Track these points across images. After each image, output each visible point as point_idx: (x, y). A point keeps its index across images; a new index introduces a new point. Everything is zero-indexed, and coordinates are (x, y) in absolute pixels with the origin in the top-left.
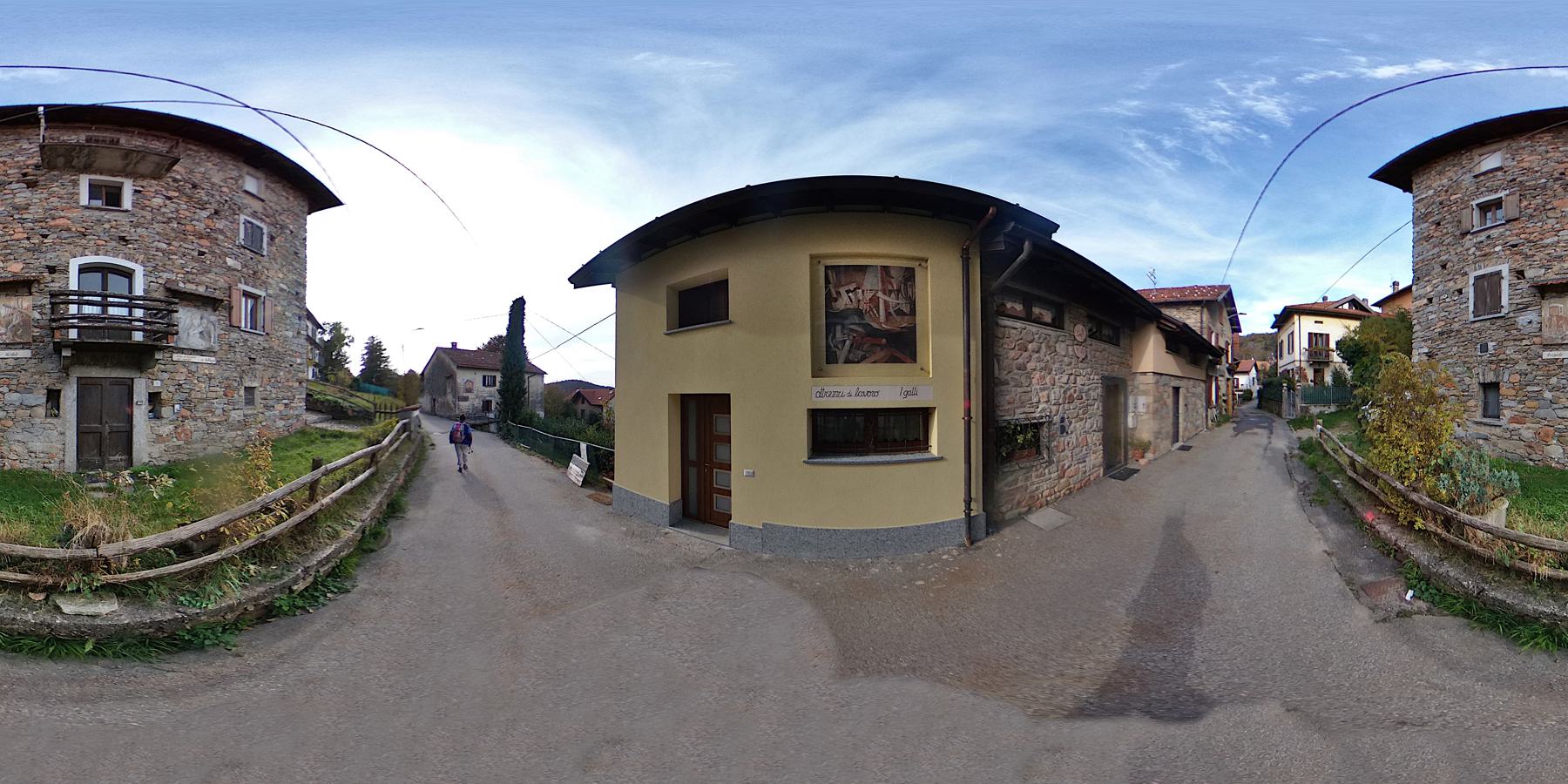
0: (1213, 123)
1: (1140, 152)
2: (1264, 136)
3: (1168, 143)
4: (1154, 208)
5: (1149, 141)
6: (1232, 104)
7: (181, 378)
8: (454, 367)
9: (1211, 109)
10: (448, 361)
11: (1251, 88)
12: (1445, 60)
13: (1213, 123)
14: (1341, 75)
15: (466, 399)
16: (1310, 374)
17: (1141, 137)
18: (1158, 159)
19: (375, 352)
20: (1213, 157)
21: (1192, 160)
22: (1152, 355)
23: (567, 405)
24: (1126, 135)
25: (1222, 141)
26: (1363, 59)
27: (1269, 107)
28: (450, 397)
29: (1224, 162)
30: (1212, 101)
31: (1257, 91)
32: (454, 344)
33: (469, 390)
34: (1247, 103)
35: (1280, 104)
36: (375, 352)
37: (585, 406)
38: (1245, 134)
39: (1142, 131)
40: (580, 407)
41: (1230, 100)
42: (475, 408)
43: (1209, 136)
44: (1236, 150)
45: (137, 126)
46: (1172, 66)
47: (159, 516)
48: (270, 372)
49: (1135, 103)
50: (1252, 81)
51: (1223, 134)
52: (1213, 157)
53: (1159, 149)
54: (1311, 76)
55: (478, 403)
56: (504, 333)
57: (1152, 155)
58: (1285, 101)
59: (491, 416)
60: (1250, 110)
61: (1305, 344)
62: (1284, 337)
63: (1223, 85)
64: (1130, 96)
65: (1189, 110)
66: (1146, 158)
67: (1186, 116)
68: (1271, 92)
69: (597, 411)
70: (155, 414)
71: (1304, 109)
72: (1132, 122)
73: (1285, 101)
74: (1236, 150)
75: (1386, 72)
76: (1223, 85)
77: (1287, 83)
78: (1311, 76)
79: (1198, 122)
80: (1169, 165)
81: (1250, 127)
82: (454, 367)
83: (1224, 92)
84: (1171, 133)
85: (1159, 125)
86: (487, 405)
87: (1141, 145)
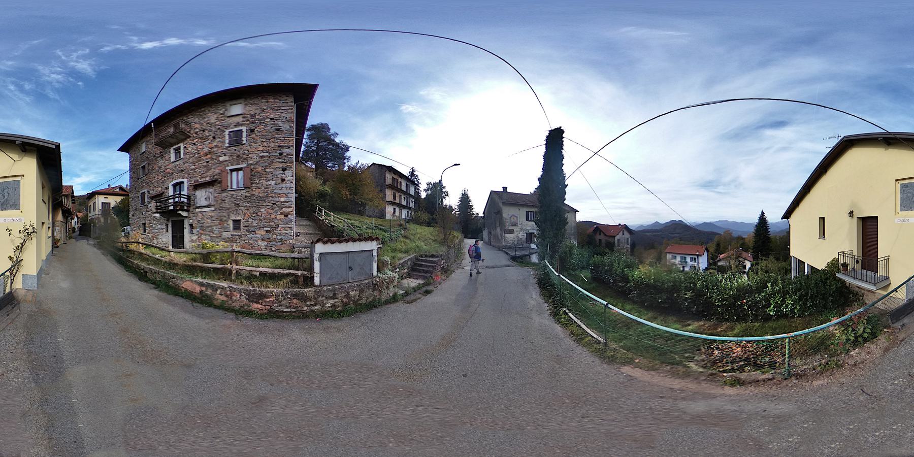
0: (53, 76)
1: (10, 91)
2: (80, 83)
3: (27, 86)
5: (16, 85)
6: (64, 64)
7: (199, 218)
8: (501, 205)
10: (500, 200)
11: (75, 55)
13: (53, 75)
14: (123, 48)
15: (511, 232)
16: (102, 220)
17: (13, 83)
18: (21, 95)
20: (51, 95)
22: (60, 217)
23: (589, 236)
24: (4, 81)
25: (57, 85)
26: (135, 38)
27: (84, 66)
28: (498, 230)
29: (57, 97)
31: (77, 57)
32: (505, 188)
33: (515, 225)
34: (72, 63)
35: (90, 65)
37: (602, 237)
38: (69, 82)
39: (13, 79)
40: (598, 237)
42: (519, 240)
43: (50, 83)
46: (35, 42)
48: (252, 210)
49: (10, 63)
50: (75, 51)
51: (58, 82)
52: (51, 95)
53: (21, 89)
54: (108, 48)
55: (522, 235)
57: (17, 93)
58: (93, 63)
59: (533, 246)
60: (73, 67)
61: (100, 207)
62: (91, 203)
63: (60, 53)
64: (9, 59)
65: (40, 68)
66: (15, 95)
67: (37, 71)
68: (85, 57)
69: (611, 240)
72: (8, 74)
73: (93, 63)
74: (65, 91)
76: (60, 53)
78: (108, 48)
80: (28, 99)
82: (501, 205)
83: (60, 57)
86: (530, 237)
87: (12, 87)
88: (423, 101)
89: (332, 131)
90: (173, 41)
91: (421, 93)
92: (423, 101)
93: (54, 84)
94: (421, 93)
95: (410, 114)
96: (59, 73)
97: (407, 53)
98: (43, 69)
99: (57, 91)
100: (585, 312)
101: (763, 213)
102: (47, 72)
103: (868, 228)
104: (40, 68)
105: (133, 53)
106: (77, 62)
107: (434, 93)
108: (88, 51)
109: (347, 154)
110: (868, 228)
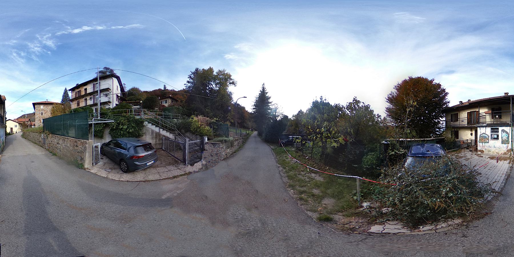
1: (14, 56)
2: (49, 52)
6: (40, 42)
11: (45, 37)
14: (66, 33)
17: (15, 52)
18: (19, 59)
19: (263, 100)
20: (33, 57)
21: (29, 59)
24: (11, 51)
25: (38, 54)
26: (69, 27)
27: (50, 43)
29: (38, 60)
34: (44, 42)
35: (53, 43)
36: (263, 100)
38: (44, 51)
39: (15, 50)
43: (34, 52)
44: (41, 56)
45: (108, 157)
46: (26, 30)
49: (15, 41)
50: (45, 35)
52: (33, 57)
53: (19, 55)
54: (59, 33)
64: (15, 39)
65: (29, 44)
67: (28, 46)
68: (50, 38)
70: (428, 151)
72: (14, 47)
75: (77, 31)
77: (54, 37)
78: (59, 33)
79: (31, 48)
83: (38, 38)
84: (24, 51)
85: (21, 48)
87: (15, 55)
88: (238, 52)
89: (319, 100)
90: (86, 28)
92: (238, 52)
95: (230, 60)
96: (39, 47)
98: (31, 45)
101: (264, 89)
102: (32, 46)
104: (29, 44)
105: (71, 36)
106: (46, 41)
107: (244, 47)
108: (50, 35)
109: (270, 100)
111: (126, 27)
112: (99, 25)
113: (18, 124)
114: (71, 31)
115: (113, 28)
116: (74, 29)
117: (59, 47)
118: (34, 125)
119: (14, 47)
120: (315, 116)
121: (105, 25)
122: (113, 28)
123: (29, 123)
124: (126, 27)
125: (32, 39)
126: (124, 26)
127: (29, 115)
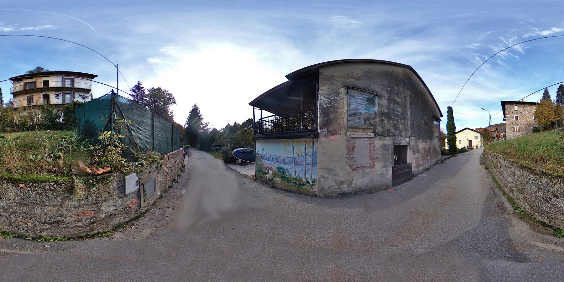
1: (477, 61)
2: (517, 57)
4: (481, 80)
9: (500, 47)
11: (510, 40)
12: (558, 28)
14: (534, 35)
17: (478, 56)
19: (195, 114)
21: (495, 65)
24: (473, 56)
25: (504, 58)
30: (500, 45)
35: (520, 46)
36: (195, 114)
39: (478, 54)
41: (505, 44)
43: (500, 57)
44: (508, 61)
46: (488, 33)
47: (91, 165)
49: (476, 45)
50: (510, 38)
56: (241, 124)
64: (476, 42)
65: (493, 47)
71: (527, 47)
72: (476, 51)
75: (545, 33)
81: (512, 53)
87: (478, 59)
88: (164, 56)
90: (556, 30)
91: (161, 50)
92: (164, 56)
93: (503, 57)
94: (161, 50)
95: (155, 64)
97: (146, 26)
99: (503, 60)
100: (49, 172)
103: (470, 142)
104: (493, 47)
107: (171, 50)
110: (470, 142)
111: (37, 28)
112: (6, 25)
113: (478, 135)
114: (539, 33)
115: (23, 29)
116: (541, 31)
117: (527, 51)
118: (505, 136)
119: (476, 51)
120: (384, 145)
121: (13, 26)
122: (23, 29)
123: (496, 133)
124: (37, 28)
125: (497, 42)
126: (34, 27)
127: (497, 126)
